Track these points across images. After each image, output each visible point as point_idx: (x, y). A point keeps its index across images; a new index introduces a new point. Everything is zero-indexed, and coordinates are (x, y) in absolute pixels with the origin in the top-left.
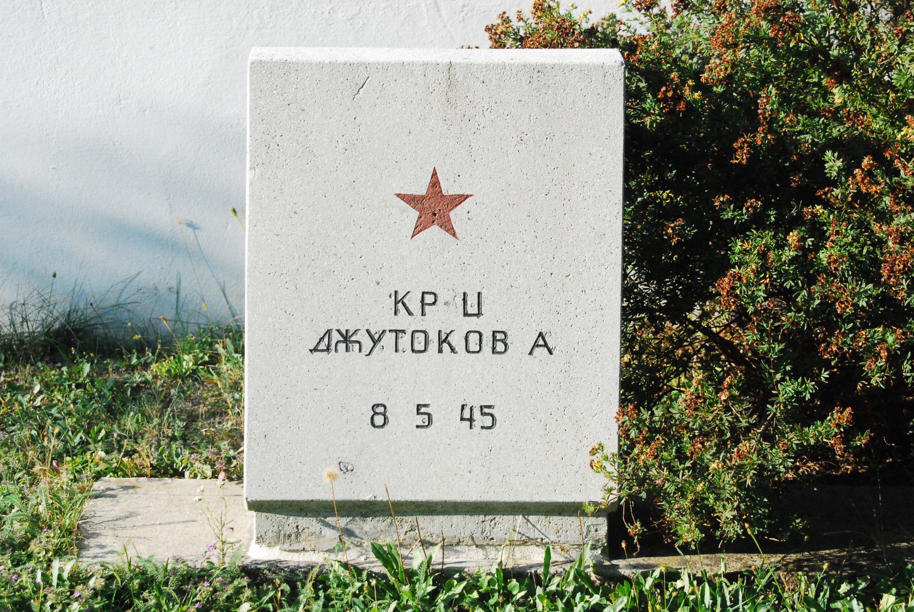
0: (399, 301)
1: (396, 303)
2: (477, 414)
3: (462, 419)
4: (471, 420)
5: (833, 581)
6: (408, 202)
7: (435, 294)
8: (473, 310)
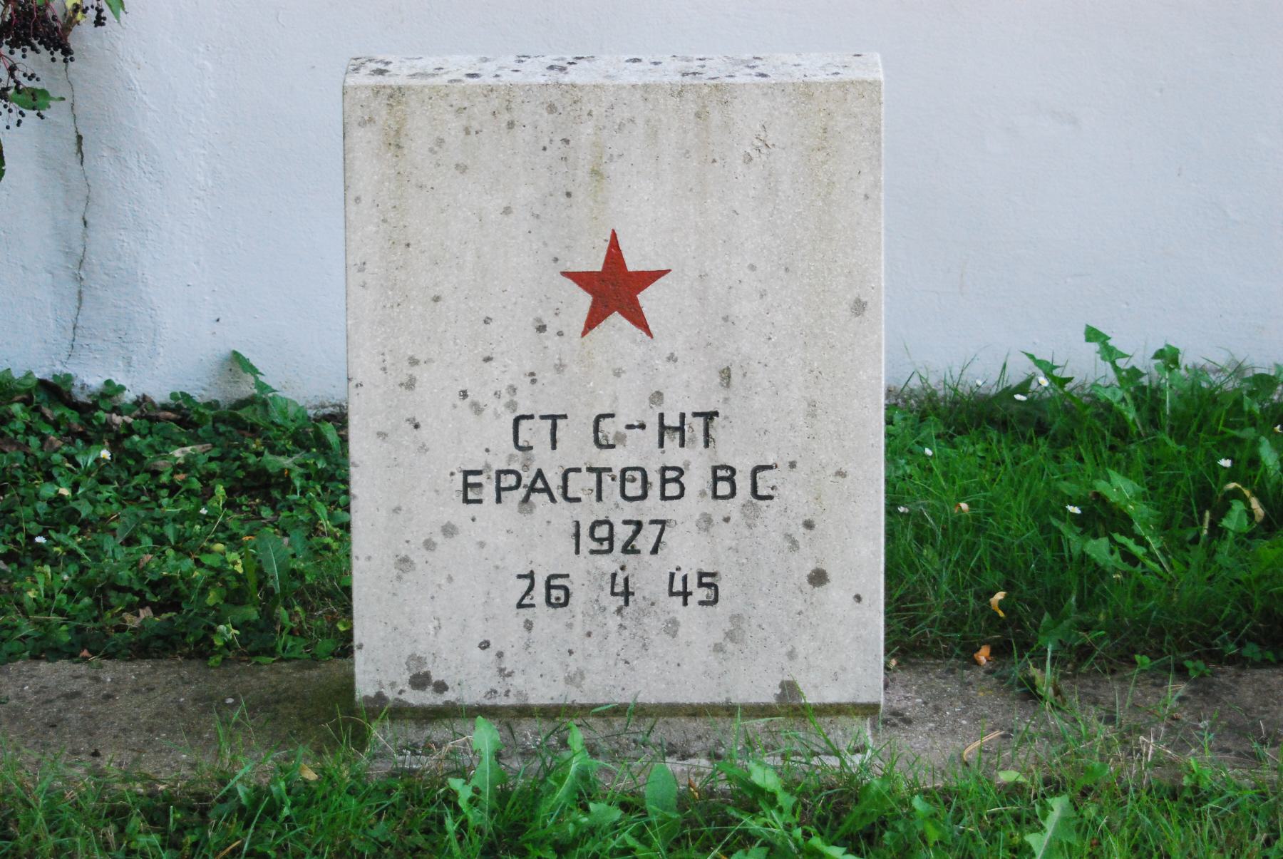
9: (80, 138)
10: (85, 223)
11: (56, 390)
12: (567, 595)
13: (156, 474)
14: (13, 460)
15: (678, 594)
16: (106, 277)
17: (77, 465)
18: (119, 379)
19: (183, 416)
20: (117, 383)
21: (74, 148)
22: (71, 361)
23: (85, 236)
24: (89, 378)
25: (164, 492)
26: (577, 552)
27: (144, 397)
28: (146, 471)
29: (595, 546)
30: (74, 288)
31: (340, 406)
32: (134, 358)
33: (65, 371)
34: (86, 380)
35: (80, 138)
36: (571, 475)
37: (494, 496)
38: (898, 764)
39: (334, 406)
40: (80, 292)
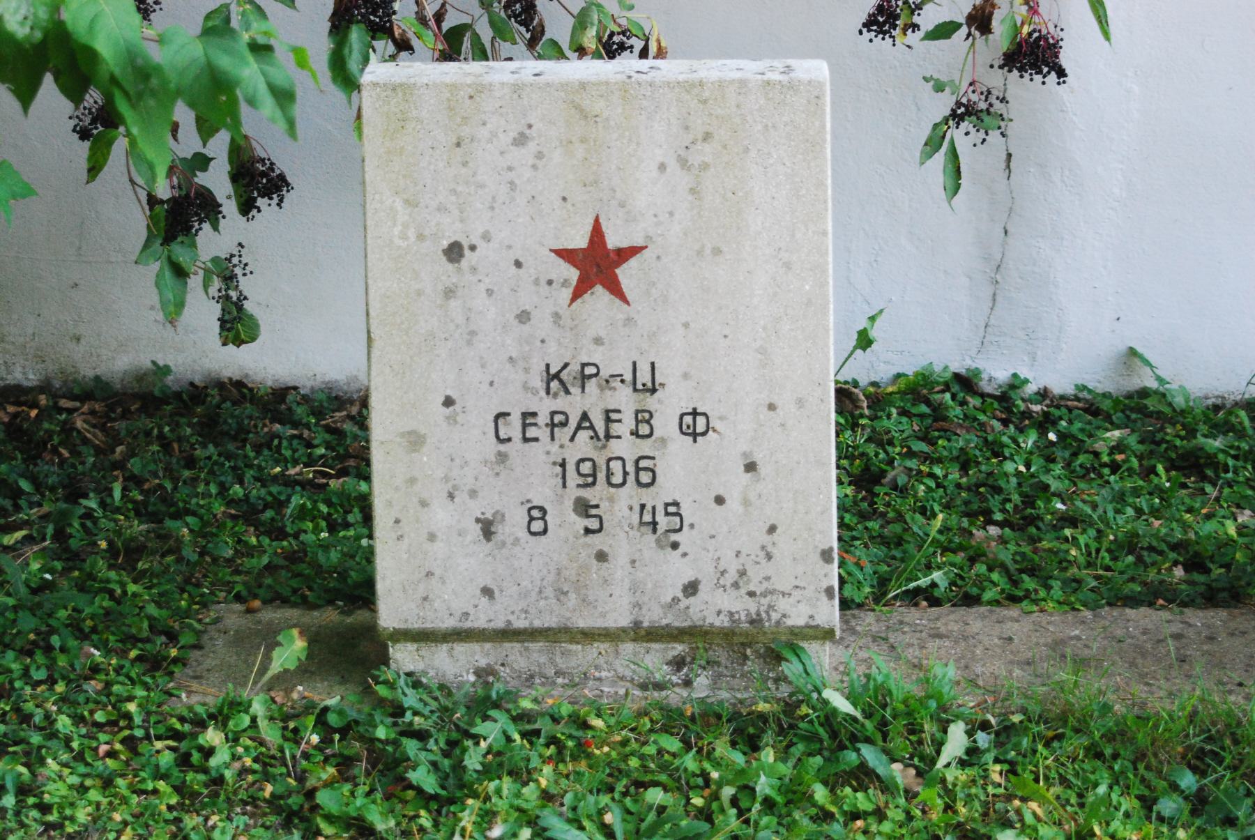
0: (552, 377)
2: (660, 517)
6: (581, 296)
9: (1009, 155)
10: (1006, 233)
11: (965, 383)
13: (1097, 454)
14: (968, 441)
16: (1019, 280)
17: (1019, 446)
18: (1024, 373)
19: (1093, 408)
20: (1022, 377)
21: (1003, 165)
22: (980, 356)
23: (1004, 244)
24: (996, 373)
25: (1106, 471)
26: (564, 486)
27: (1046, 389)
28: (1087, 452)
30: (989, 291)
31: (1223, 398)
32: (1039, 353)
33: (974, 366)
34: (993, 374)
35: (1009, 155)
38: (620, 670)
39: (1217, 397)
40: (994, 294)
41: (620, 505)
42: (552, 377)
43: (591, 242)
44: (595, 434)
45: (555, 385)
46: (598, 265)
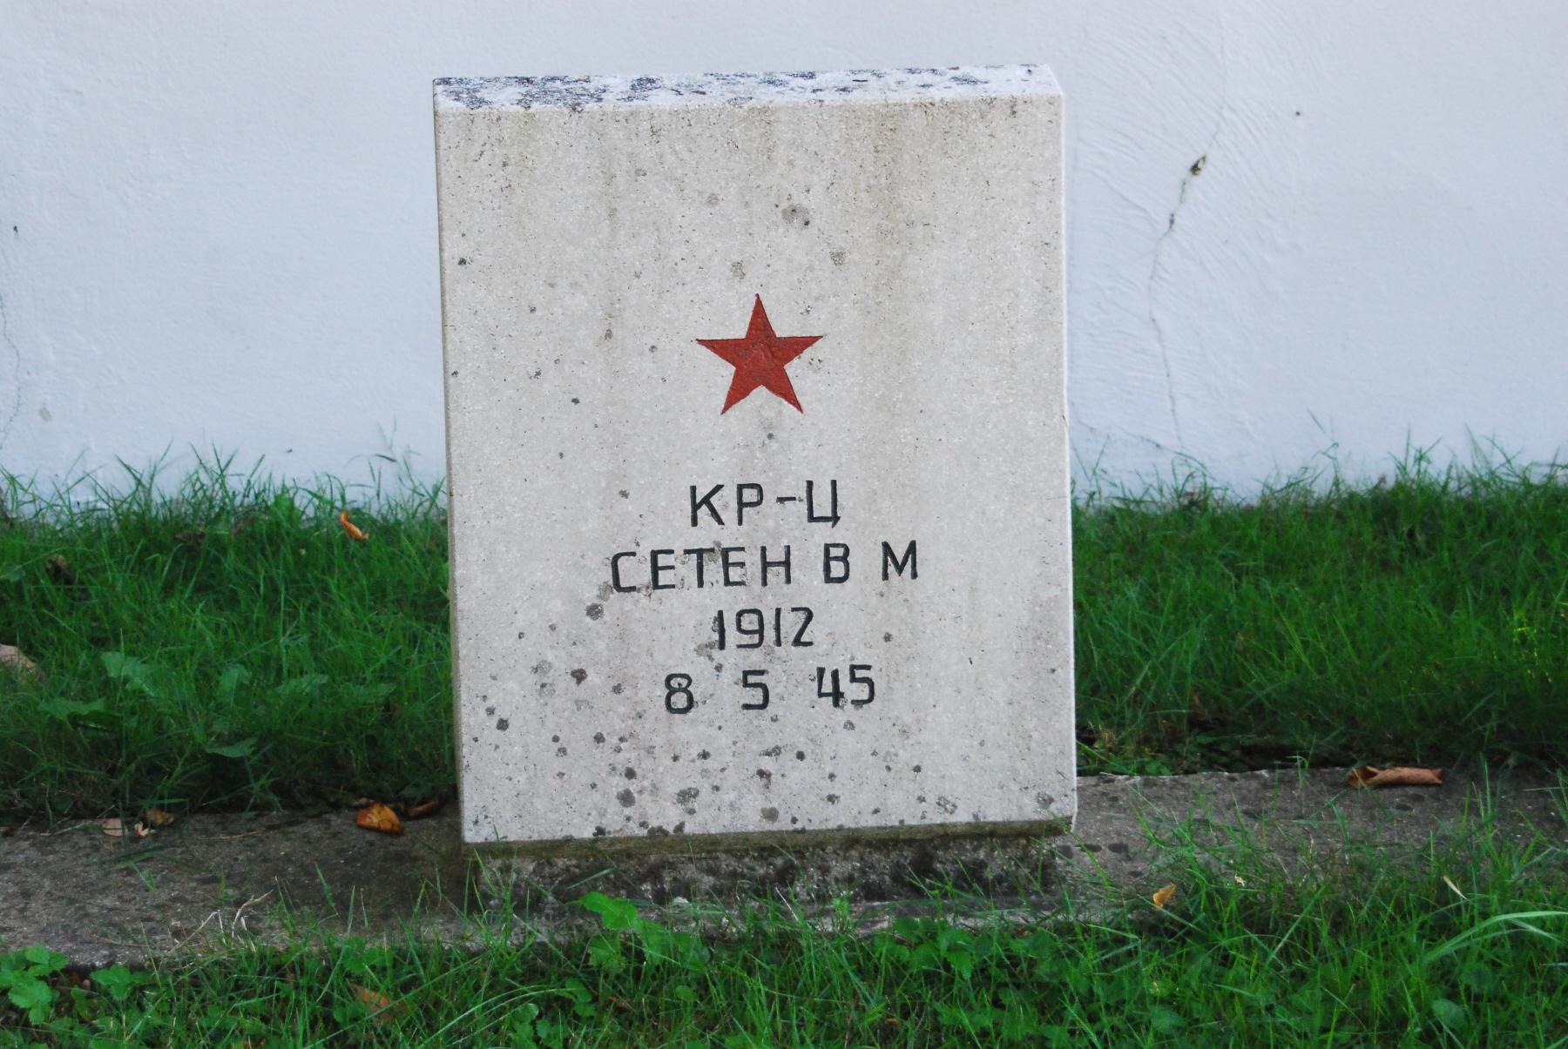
0: (701, 503)
1: (695, 507)
2: (845, 684)
3: (821, 695)
4: (837, 696)
5: (303, 552)
6: (745, 394)
7: (846, 577)
8: (823, 509)
10: (1172, 222)
12: (685, 711)
15: (827, 695)
29: (746, 639)
35: (975, 82)
36: (622, 562)
37: (759, 574)
41: (790, 671)
42: (701, 503)
43: (753, 325)
44: (754, 576)
45: (704, 512)
46: (760, 358)
